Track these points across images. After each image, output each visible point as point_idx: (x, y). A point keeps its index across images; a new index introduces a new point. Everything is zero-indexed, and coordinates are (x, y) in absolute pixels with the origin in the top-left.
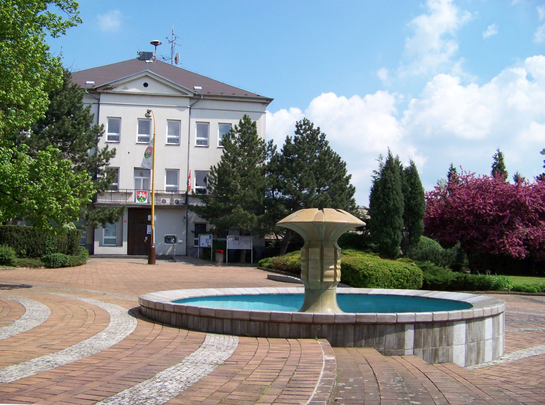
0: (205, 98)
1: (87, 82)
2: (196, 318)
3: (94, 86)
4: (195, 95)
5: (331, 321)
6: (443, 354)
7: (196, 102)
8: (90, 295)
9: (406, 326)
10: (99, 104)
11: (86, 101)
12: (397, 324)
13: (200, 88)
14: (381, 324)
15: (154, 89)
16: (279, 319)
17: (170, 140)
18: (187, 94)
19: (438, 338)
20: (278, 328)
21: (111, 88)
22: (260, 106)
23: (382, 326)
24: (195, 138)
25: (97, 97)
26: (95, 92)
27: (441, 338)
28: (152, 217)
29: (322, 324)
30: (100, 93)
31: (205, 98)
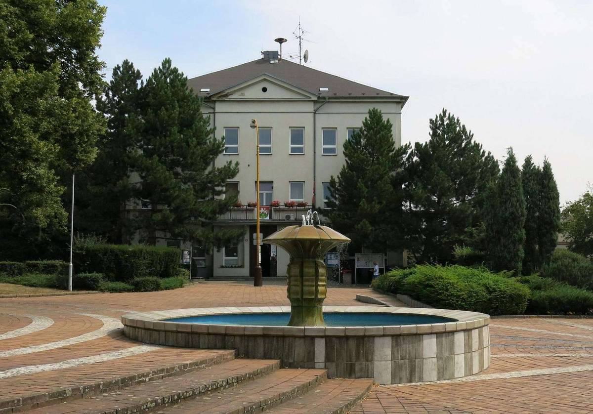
0: (331, 100)
1: (321, 89)
2: (143, 331)
3: (208, 94)
4: (319, 98)
5: (241, 333)
6: (361, 370)
7: (322, 105)
8: (86, 312)
9: (317, 340)
10: (214, 113)
11: (205, 111)
12: (305, 337)
13: (327, 89)
14: (289, 336)
15: (274, 93)
16: (199, 331)
17: (293, 150)
18: (310, 98)
19: (354, 353)
20: (199, 340)
21: (226, 96)
22: (394, 105)
23: (291, 339)
24: (321, 146)
25: (212, 105)
26: (209, 100)
27: (358, 353)
28: (257, 235)
29: (235, 336)
30: (215, 102)
31: (331, 100)
